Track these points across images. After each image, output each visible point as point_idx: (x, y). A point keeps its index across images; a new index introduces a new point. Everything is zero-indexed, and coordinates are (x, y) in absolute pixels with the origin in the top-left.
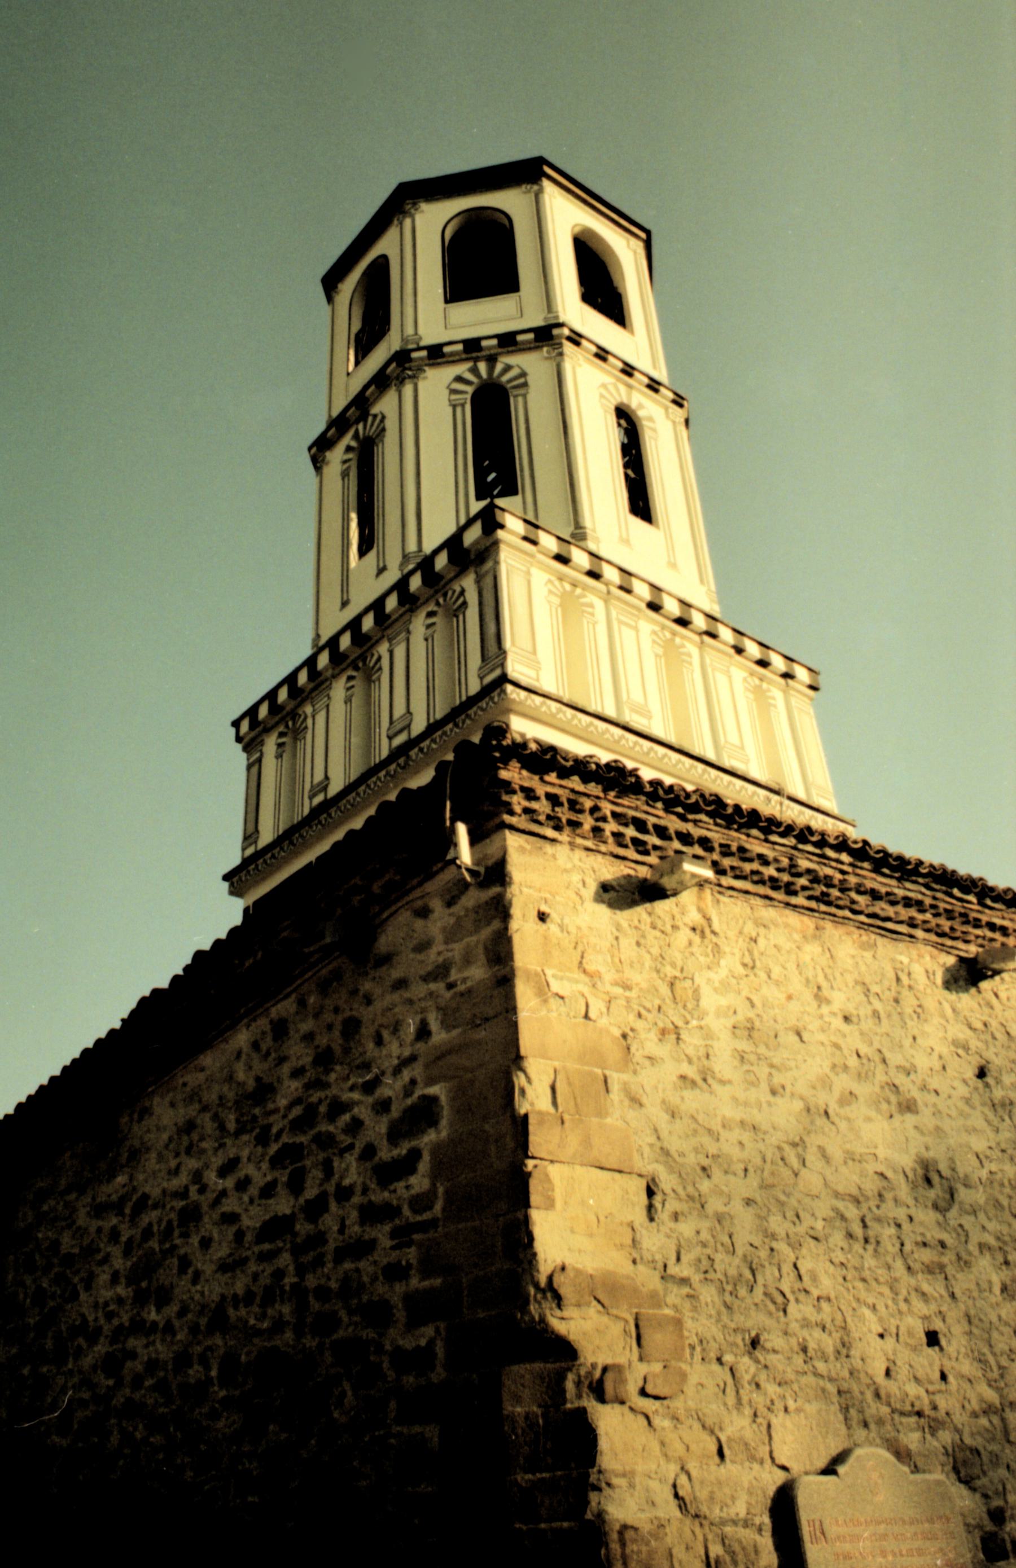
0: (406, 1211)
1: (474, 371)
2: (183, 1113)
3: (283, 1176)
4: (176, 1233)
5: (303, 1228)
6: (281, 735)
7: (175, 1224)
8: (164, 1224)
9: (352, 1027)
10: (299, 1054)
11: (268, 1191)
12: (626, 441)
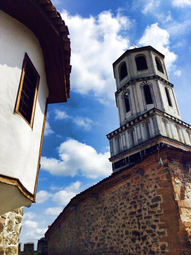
0: (157, 212)
1: (144, 83)
2: (111, 195)
3: (133, 206)
4: (113, 213)
5: (137, 214)
6: (115, 138)
7: (113, 211)
8: (111, 211)
9: (142, 185)
10: (132, 188)
11: (130, 208)
12: (68, 36)
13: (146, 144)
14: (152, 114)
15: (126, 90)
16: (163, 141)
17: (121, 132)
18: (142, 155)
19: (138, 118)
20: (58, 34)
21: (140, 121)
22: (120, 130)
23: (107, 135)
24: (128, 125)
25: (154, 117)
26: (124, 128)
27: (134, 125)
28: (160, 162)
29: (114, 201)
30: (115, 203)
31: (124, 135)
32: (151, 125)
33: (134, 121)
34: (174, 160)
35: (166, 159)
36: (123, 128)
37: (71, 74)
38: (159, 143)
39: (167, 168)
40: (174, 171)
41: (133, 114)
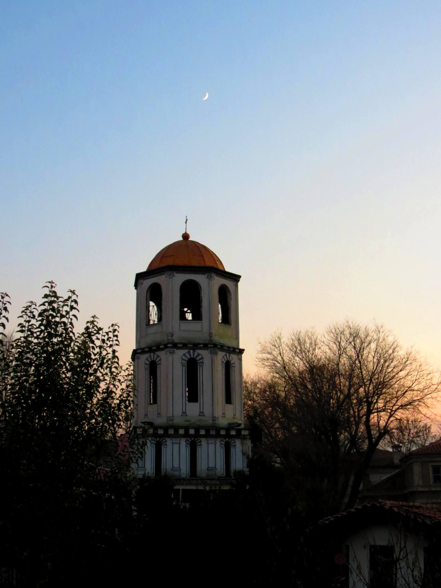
1: (189, 352)
14: (244, 435)
17: (170, 436)
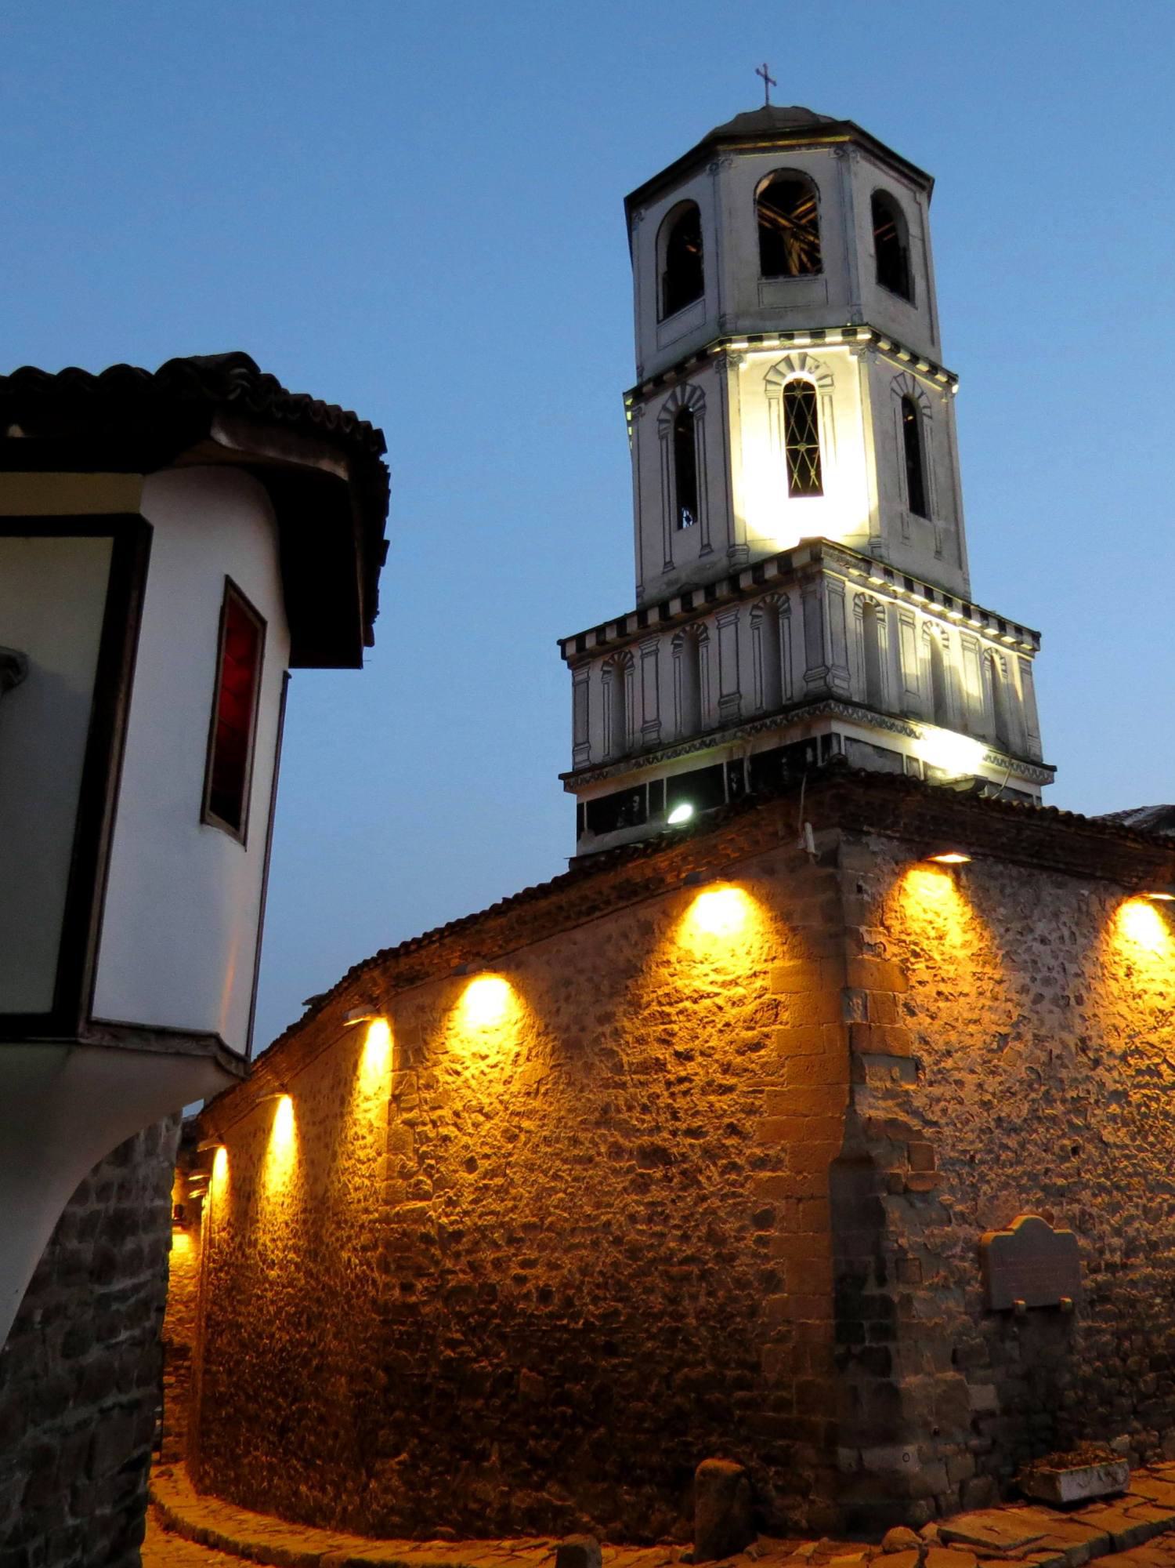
6: (606, 663)
13: (758, 731)
14: (804, 568)
15: (688, 389)
16: (837, 728)
17: (636, 640)
18: (730, 780)
19: (733, 579)
20: (359, 565)
21: (739, 595)
22: (632, 627)
23: (562, 643)
24: (675, 607)
25: (811, 587)
26: (653, 617)
27: (707, 612)
28: (806, 841)
29: (567, 998)
30: (572, 1008)
31: (653, 658)
32: (794, 626)
33: (709, 589)
34: (872, 830)
35: (833, 826)
36: (650, 622)
37: (383, 569)
38: (818, 733)
39: (831, 870)
40: (865, 887)
41: (709, 545)
